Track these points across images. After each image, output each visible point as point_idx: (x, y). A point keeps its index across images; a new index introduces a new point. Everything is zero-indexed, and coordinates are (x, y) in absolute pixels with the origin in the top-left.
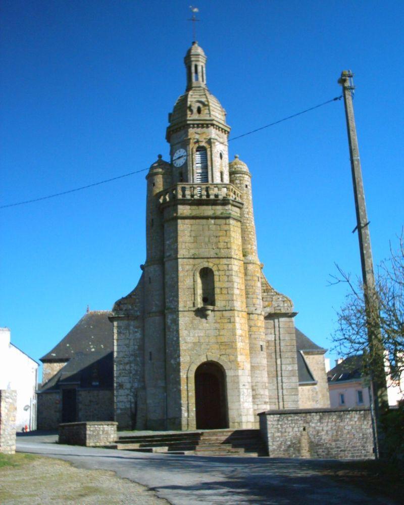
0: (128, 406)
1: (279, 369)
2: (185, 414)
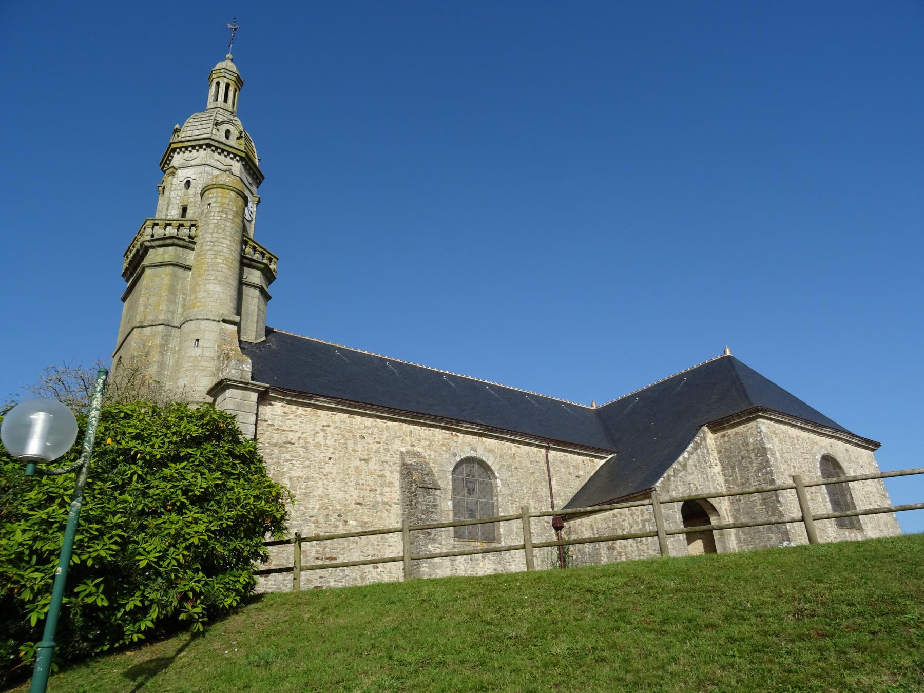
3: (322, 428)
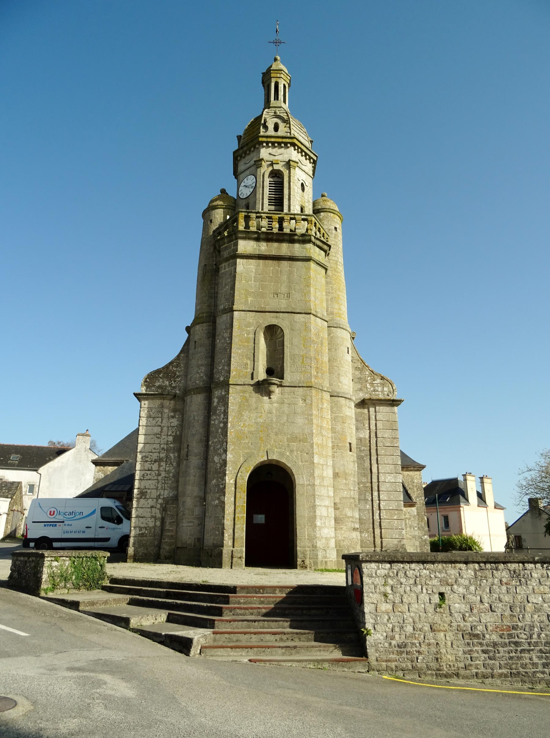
0: (151, 524)
1: (375, 480)
2: (228, 541)
3: (125, 520)
